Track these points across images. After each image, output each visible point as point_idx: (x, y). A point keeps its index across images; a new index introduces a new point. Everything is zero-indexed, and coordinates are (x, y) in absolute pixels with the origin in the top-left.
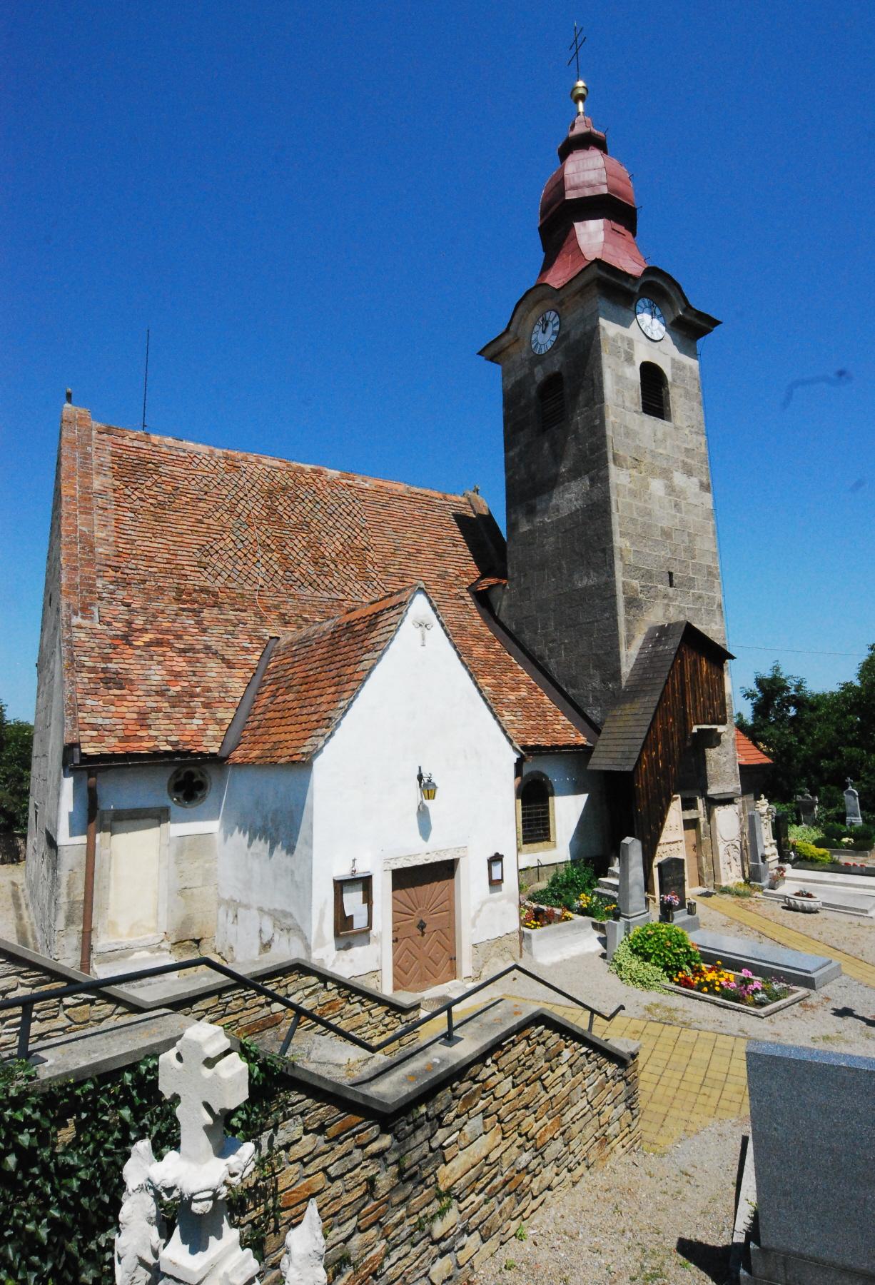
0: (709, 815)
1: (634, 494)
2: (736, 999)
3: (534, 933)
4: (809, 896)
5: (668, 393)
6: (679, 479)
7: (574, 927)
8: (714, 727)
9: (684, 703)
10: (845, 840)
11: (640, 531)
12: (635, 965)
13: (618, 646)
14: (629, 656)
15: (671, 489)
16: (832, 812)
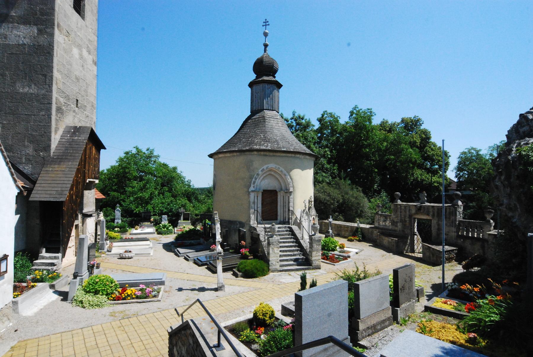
0: (83, 222)
1: (65, 50)
2: (145, 298)
3: (19, 299)
4: (130, 252)
5: (84, 5)
6: (85, 53)
7: (40, 290)
8: (94, 180)
9: (85, 168)
10: (116, 229)
11: (66, 72)
12: (90, 298)
13: (50, 132)
14: (56, 139)
15: (81, 57)
16: (109, 218)
